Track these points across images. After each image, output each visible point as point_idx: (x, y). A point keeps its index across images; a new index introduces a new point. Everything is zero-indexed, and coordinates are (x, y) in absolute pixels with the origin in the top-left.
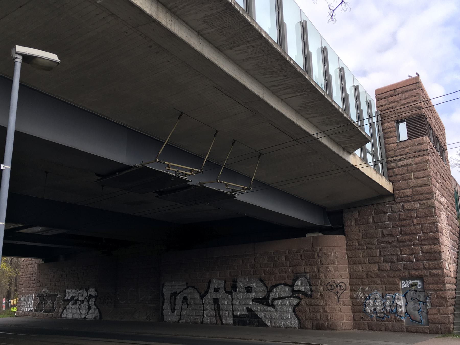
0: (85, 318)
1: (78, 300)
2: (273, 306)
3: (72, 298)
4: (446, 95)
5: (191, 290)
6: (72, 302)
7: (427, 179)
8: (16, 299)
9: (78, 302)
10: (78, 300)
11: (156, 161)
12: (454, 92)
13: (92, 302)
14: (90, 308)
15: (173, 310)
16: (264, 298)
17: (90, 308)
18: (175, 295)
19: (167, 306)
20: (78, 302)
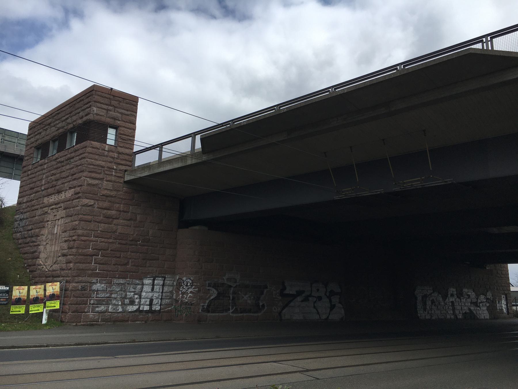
0: (327, 319)
1: (310, 296)
2: (479, 307)
3: (299, 293)
4: (22, 58)
5: (436, 294)
6: (299, 299)
7: (112, 185)
8: (43, 286)
9: (310, 299)
10: (310, 296)
11: (432, 177)
12: (28, 60)
13: (335, 300)
14: (332, 307)
15: (425, 309)
16: (476, 302)
17: (332, 307)
18: (425, 297)
19: (419, 306)
20: (310, 299)
